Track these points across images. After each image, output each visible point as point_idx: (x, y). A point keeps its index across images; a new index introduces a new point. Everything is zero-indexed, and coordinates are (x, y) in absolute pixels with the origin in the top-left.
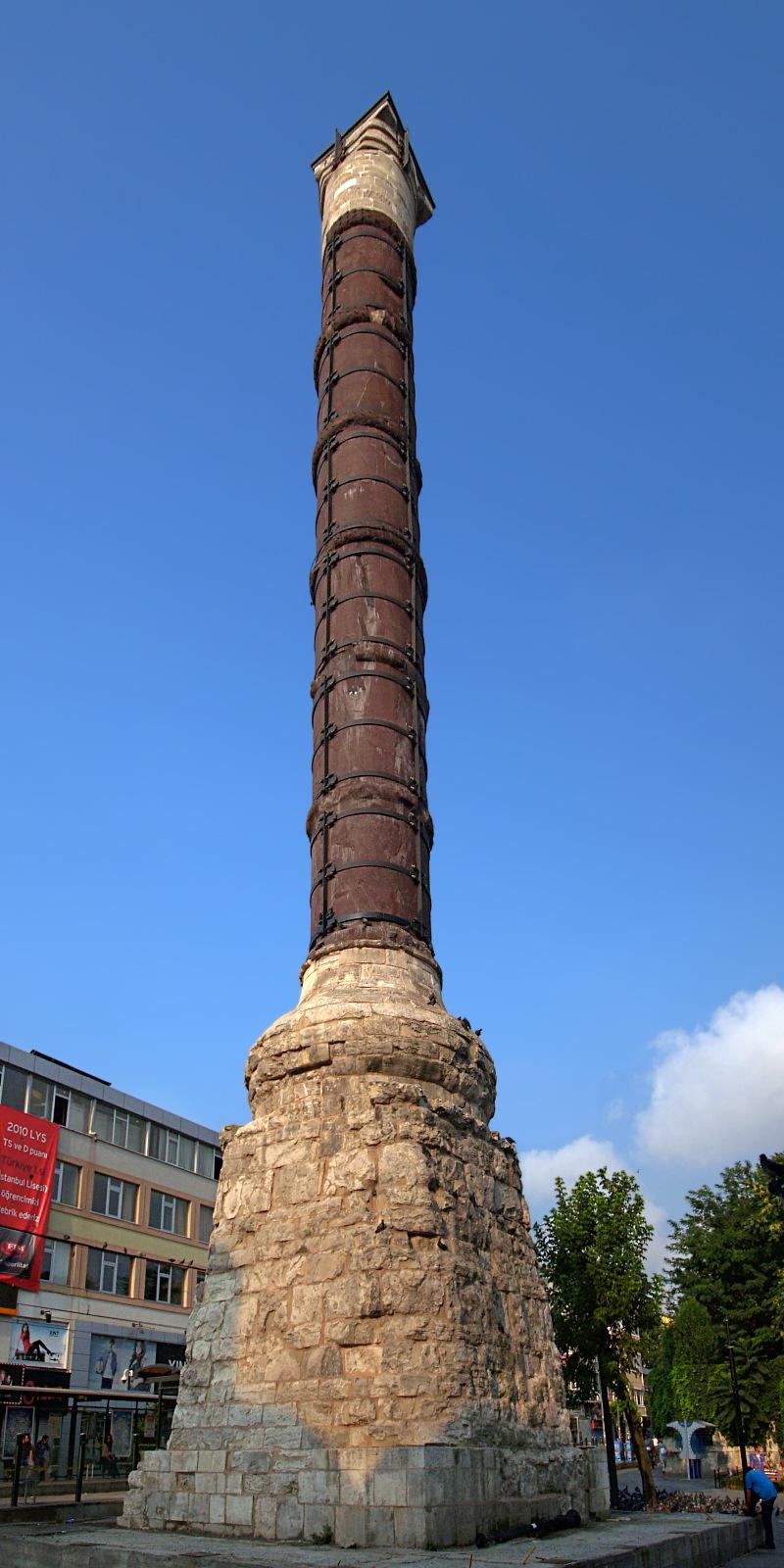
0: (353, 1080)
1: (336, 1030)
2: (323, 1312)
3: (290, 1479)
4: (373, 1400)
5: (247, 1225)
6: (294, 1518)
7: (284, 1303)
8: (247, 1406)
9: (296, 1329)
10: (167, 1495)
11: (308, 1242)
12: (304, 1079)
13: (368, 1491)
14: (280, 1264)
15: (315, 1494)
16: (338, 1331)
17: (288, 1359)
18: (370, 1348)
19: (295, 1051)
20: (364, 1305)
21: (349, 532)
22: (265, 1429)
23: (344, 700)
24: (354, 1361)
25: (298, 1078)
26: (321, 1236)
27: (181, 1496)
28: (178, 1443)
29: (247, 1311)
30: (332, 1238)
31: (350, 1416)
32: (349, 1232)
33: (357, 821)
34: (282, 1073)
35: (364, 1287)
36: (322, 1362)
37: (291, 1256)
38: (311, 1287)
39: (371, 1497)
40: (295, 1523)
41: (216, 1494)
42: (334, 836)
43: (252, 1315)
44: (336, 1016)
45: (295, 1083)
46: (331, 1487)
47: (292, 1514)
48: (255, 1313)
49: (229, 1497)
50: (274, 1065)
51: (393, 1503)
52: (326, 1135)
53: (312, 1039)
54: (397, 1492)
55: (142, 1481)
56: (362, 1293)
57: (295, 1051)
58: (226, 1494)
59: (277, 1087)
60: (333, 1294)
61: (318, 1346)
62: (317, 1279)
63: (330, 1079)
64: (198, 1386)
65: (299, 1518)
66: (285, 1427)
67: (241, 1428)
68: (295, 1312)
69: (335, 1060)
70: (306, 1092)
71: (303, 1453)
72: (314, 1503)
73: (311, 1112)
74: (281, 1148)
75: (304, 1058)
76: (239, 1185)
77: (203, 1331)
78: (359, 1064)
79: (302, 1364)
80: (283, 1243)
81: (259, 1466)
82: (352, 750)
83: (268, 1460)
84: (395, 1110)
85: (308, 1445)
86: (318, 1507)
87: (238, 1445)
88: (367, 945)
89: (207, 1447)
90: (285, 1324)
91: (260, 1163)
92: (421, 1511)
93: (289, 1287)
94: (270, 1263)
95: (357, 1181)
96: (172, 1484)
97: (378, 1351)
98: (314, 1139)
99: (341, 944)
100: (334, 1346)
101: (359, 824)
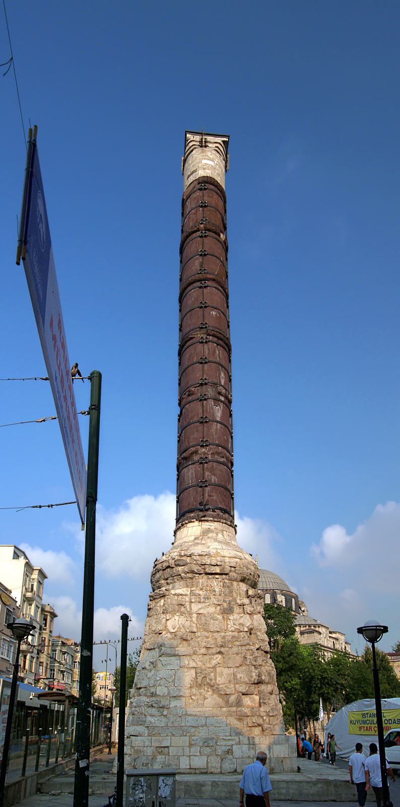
0: (235, 583)
1: (233, 562)
2: (235, 679)
3: (227, 748)
4: (262, 717)
5: (184, 637)
6: (231, 764)
7: (212, 674)
8: (196, 718)
9: (220, 686)
10: (150, 758)
11: (222, 649)
12: (214, 578)
13: (270, 752)
14: (207, 657)
15: (242, 754)
16: (242, 688)
17: (217, 698)
18: (253, 696)
19: (213, 565)
20: (255, 679)
21: (215, 333)
22: (208, 727)
23: (212, 408)
24: (247, 701)
25: (210, 576)
26: (230, 648)
27: (160, 758)
28: (153, 733)
29: (188, 677)
30: (235, 649)
31: (254, 723)
32: (243, 648)
33: (219, 466)
34: (202, 572)
35: (254, 672)
36: (236, 701)
37: (213, 654)
38: (227, 669)
39: (271, 754)
40: (232, 766)
41: (183, 756)
42: (207, 468)
43: (193, 678)
44: (232, 556)
45: (209, 579)
46: (251, 751)
47: (230, 762)
48: (194, 676)
49: (192, 757)
50: (200, 568)
51: (282, 756)
52: (225, 605)
53: (223, 563)
54: (284, 752)
55: (131, 751)
56: (254, 674)
57: (213, 565)
58: (190, 756)
59: (197, 577)
60: (239, 673)
61: (234, 694)
62: (230, 666)
63: (226, 581)
64: (163, 707)
65: (234, 764)
66: (220, 727)
67: (194, 727)
68: (218, 678)
69: (231, 573)
70: (216, 584)
71: (233, 738)
72: (242, 758)
73: (218, 593)
74: (200, 606)
75: (218, 570)
76: (176, 618)
77: (162, 682)
78: (239, 578)
79: (227, 702)
80: (207, 648)
81: (206, 743)
82: (216, 433)
83: (214, 740)
84: (256, 601)
85: (234, 735)
86: (244, 760)
87: (193, 734)
88: (225, 523)
89: (173, 735)
90: (214, 683)
91: (188, 609)
92: (295, 758)
93: (214, 667)
94: (201, 656)
95: (245, 628)
96: (153, 752)
97: (257, 698)
98: (219, 605)
99: (216, 519)
100: (241, 694)
101: (219, 468)
